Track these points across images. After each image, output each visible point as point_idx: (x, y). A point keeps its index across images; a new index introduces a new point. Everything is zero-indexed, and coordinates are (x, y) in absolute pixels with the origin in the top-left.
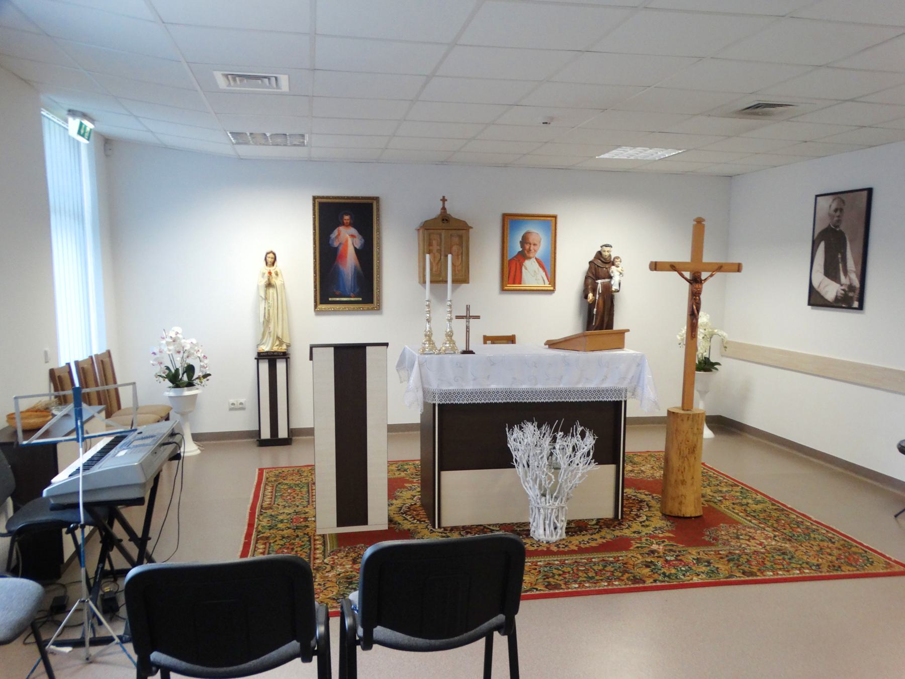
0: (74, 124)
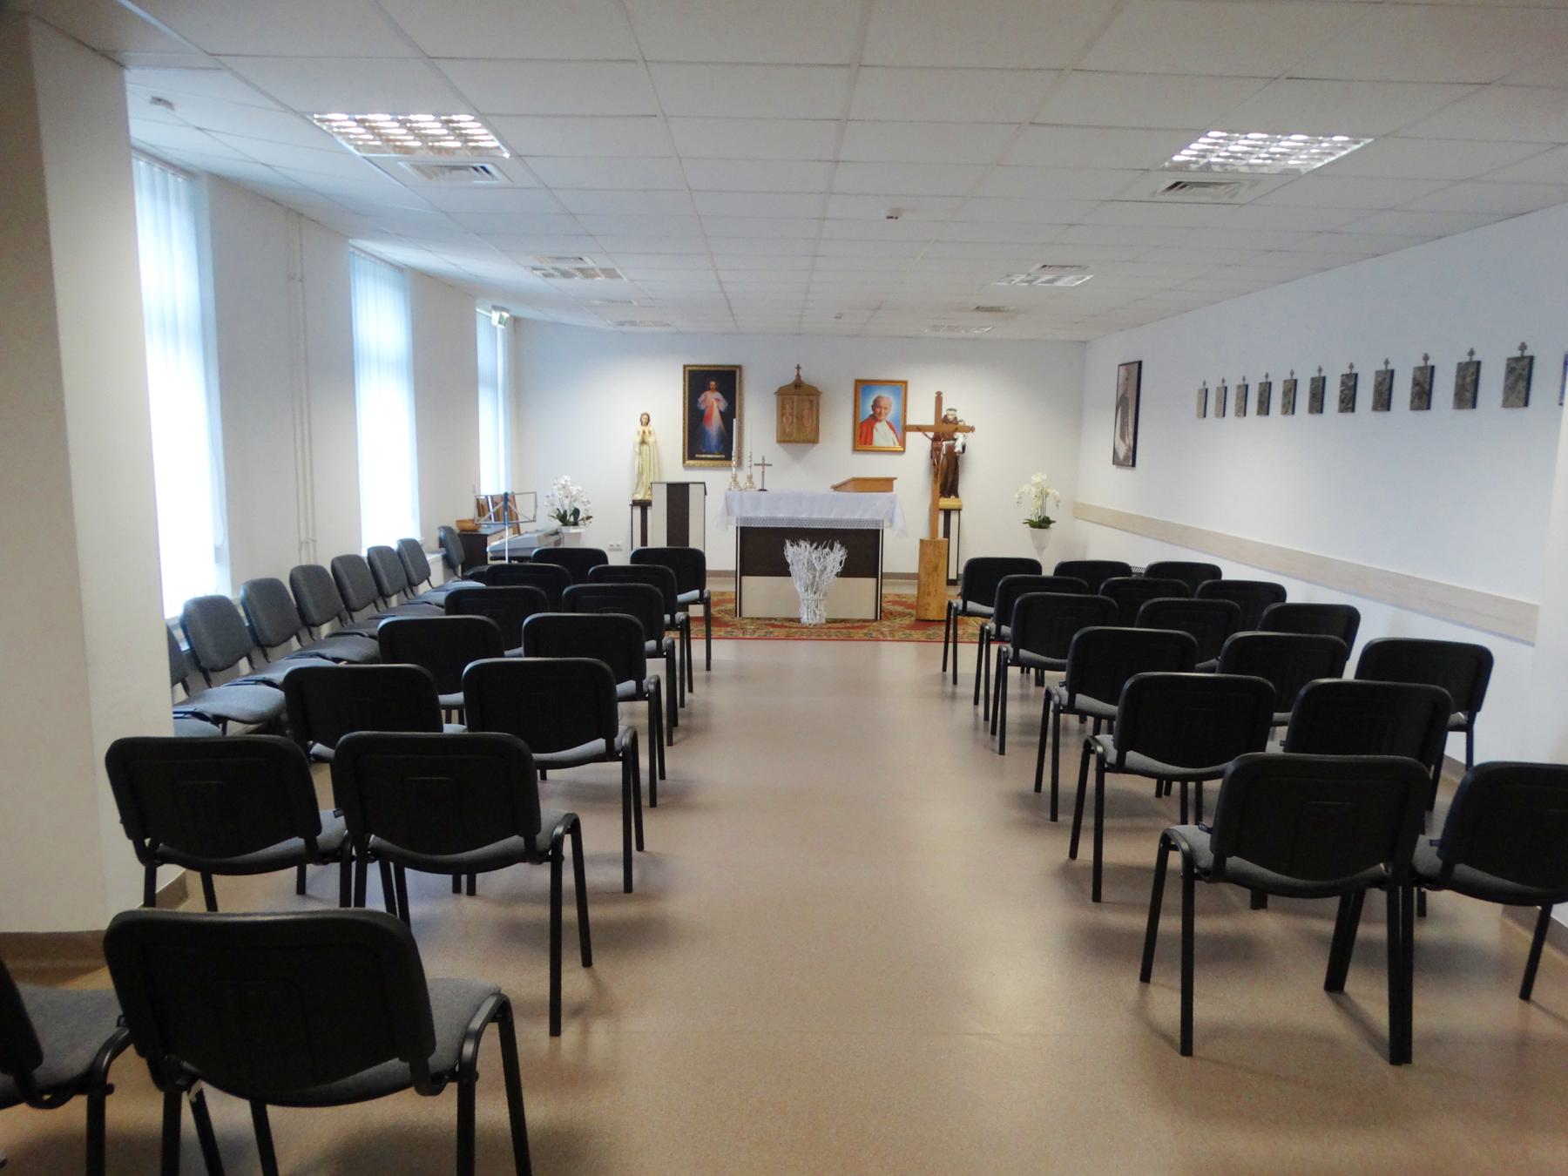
0: (495, 316)
